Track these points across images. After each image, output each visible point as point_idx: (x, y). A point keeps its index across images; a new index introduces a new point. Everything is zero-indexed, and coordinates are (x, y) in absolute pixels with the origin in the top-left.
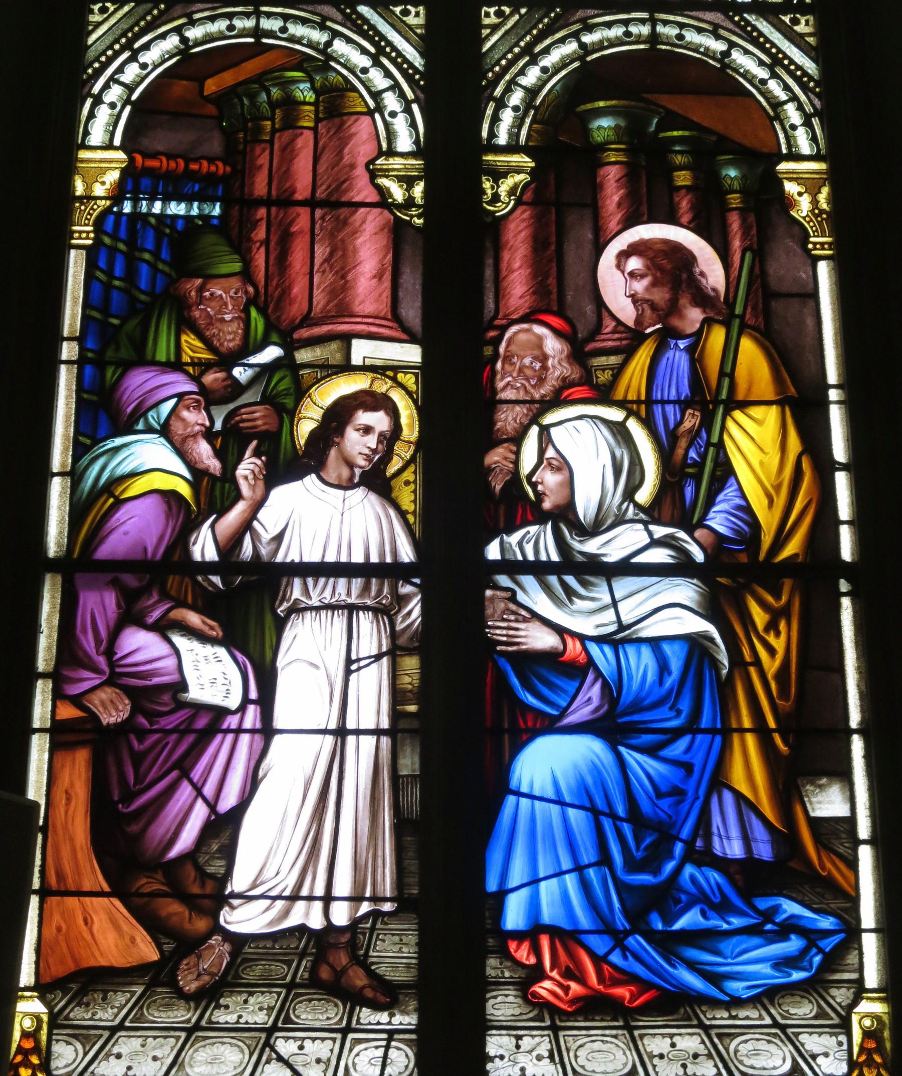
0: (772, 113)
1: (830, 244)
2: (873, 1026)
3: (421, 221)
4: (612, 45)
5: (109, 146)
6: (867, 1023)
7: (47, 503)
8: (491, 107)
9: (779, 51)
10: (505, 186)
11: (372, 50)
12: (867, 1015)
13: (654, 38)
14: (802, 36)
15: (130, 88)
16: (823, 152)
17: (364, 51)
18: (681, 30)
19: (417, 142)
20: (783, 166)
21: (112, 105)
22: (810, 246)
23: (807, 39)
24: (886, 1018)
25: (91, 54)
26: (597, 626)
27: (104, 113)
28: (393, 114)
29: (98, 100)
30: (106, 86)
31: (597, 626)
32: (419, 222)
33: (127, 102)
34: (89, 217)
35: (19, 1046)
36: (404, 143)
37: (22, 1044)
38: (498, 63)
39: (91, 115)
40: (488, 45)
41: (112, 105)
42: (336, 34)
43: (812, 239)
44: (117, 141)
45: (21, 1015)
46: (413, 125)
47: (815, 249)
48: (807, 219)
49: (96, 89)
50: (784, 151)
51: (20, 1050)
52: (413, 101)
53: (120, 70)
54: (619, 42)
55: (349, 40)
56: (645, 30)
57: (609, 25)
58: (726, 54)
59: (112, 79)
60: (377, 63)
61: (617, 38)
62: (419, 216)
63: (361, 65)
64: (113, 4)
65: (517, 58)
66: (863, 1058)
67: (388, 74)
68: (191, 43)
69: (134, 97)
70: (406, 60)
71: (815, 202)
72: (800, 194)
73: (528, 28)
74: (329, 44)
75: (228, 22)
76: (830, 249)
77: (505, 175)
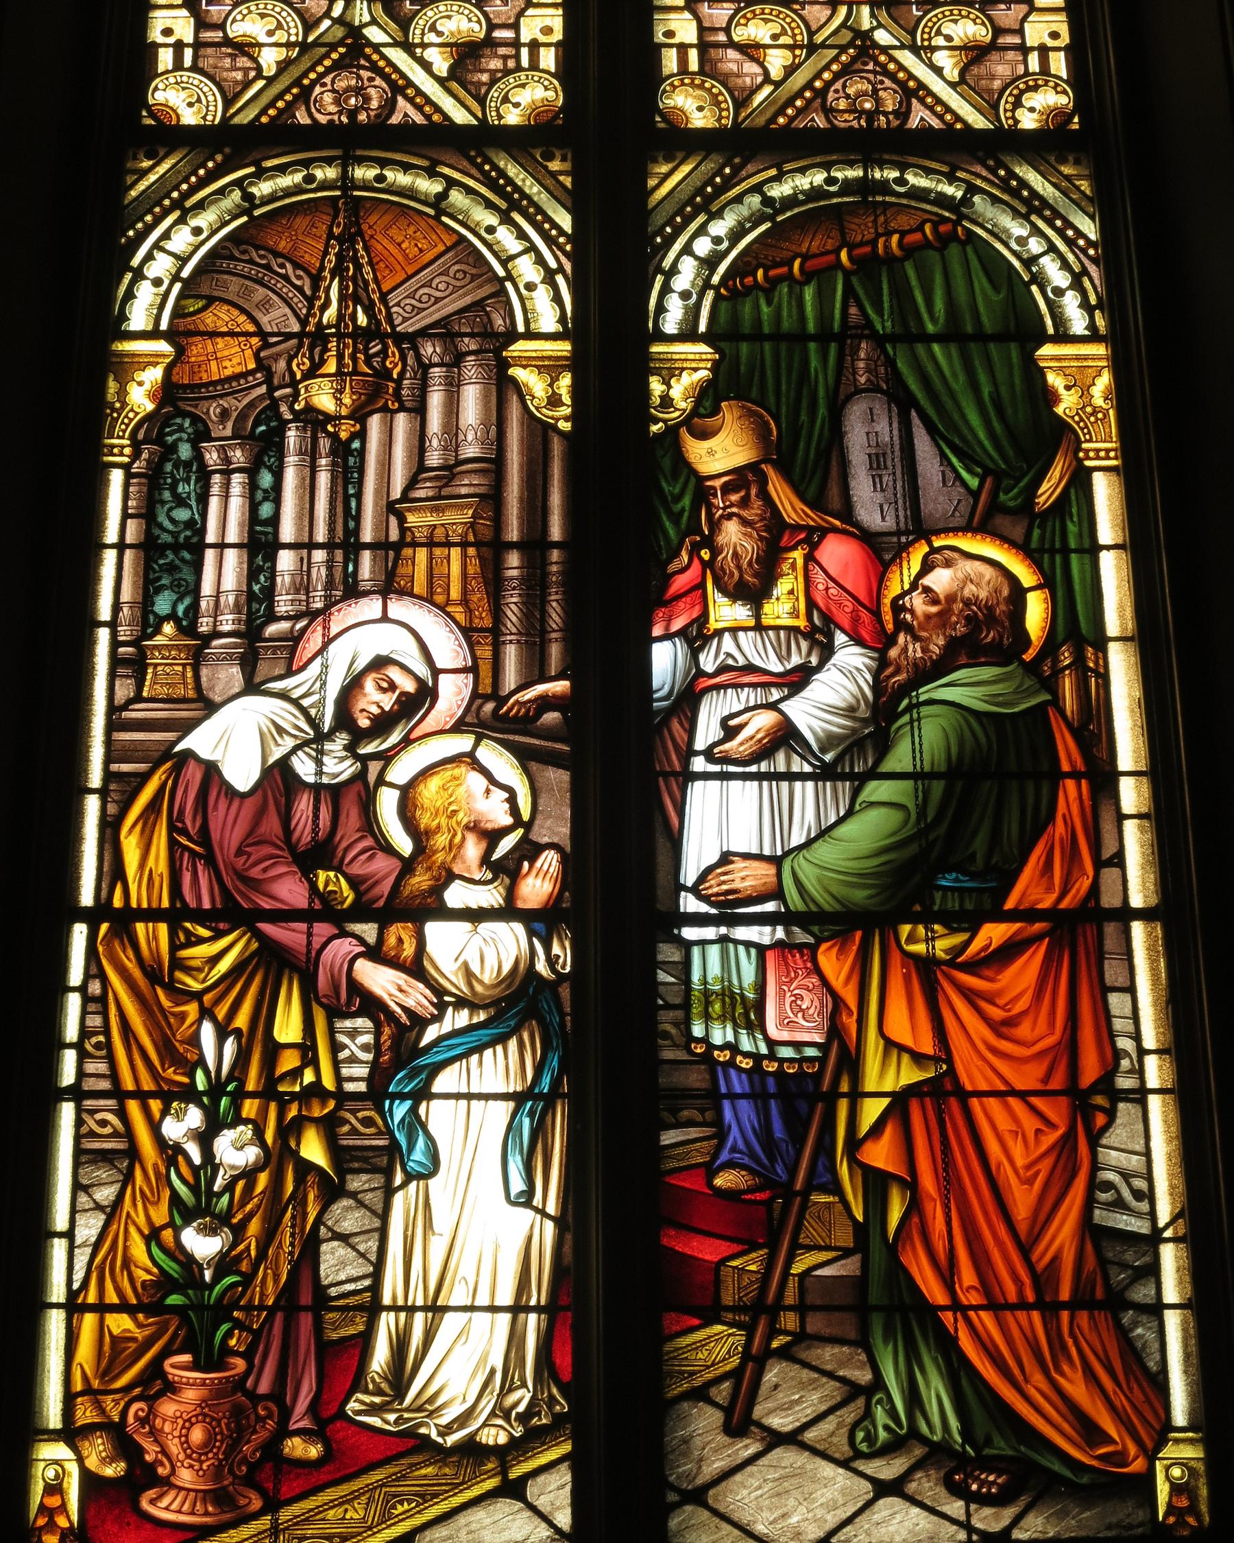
0: (501, 272)
1: (1115, 450)
2: (1182, 1478)
3: (569, 424)
6: (1176, 1472)
11: (503, 205)
12: (1178, 1462)
13: (346, 183)
14: (554, 175)
15: (183, 260)
17: (489, 205)
18: (829, 172)
19: (562, 320)
20: (1047, 350)
21: (157, 282)
22: (1081, 455)
23: (561, 178)
24: (1201, 1467)
26: (456, 959)
27: (146, 294)
28: (530, 287)
29: (139, 275)
30: (149, 257)
31: (456, 959)
32: (565, 426)
33: (176, 278)
35: (42, 1504)
36: (548, 321)
39: (130, 295)
41: (157, 282)
42: (451, 183)
43: (1085, 446)
45: (42, 1465)
46: (557, 299)
47: (1088, 458)
48: (1077, 418)
49: (135, 262)
50: (1051, 331)
51: (42, 1508)
52: (662, 272)
53: (166, 236)
54: (297, 190)
55: (469, 191)
56: (331, 173)
57: (282, 169)
58: (966, 201)
59: (157, 246)
60: (506, 220)
61: (296, 186)
62: (566, 419)
63: (487, 223)
65: (166, 212)
66: (1172, 1520)
67: (522, 235)
68: (257, 202)
74: (443, 196)
75: (378, 171)
76: (1116, 458)
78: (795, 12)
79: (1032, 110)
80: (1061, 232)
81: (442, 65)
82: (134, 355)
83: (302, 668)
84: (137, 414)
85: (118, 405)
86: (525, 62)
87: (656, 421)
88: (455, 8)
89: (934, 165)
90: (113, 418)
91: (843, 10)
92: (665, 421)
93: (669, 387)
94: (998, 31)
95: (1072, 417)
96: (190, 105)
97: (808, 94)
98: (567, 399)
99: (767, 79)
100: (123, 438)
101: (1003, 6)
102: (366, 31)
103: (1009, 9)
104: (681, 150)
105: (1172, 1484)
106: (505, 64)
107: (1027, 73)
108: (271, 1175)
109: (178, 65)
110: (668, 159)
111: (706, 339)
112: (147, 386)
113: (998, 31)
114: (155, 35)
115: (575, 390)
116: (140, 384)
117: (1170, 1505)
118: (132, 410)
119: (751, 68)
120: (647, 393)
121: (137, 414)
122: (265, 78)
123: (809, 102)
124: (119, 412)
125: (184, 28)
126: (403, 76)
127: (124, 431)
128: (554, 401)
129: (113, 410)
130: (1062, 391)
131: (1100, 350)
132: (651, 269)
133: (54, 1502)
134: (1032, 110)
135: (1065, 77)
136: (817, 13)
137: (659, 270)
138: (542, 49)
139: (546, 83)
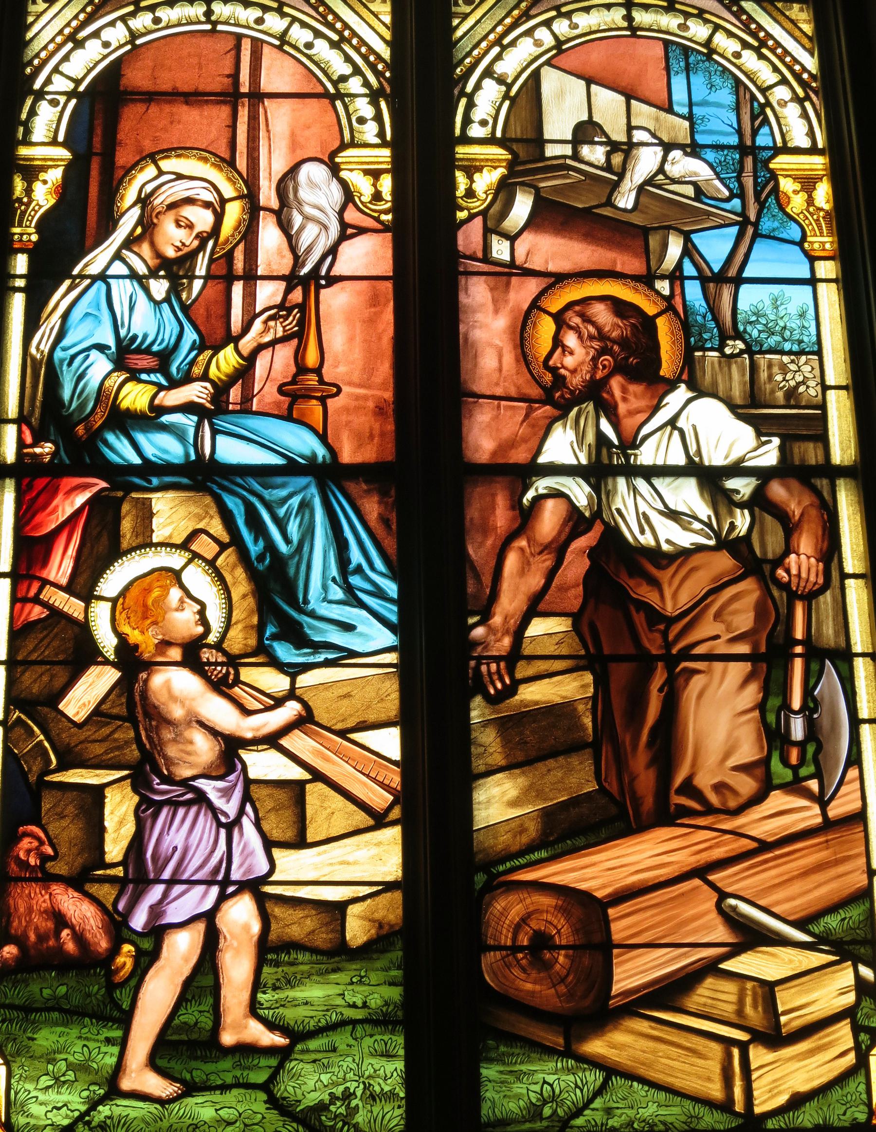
4: (190, 23)
5: (54, 142)
7: (846, 334)
8: (463, 102)
9: (346, 26)
16: (820, 145)
25: (30, 53)
34: (37, 208)
37: (108, 792)
38: (37, 55)
39: (33, 113)
40: (459, 33)
44: (61, 138)
59: (56, 70)
69: (81, 88)
70: (371, 50)
71: (810, 201)
72: (796, 192)
73: (508, 9)
77: (480, 169)
80: (781, 59)
83: (494, 595)
84: (41, 207)
85: (25, 200)
87: (462, 209)
92: (468, 209)
93: (472, 181)
95: (798, 215)
98: (389, 198)
100: (30, 227)
108: (397, 512)
110: (384, 520)
111: (64, 145)
112: (50, 185)
115: (395, 192)
116: (45, 182)
118: (38, 204)
120: (452, 185)
121: (41, 207)
124: (28, 205)
127: (31, 222)
128: (377, 196)
129: (22, 203)
132: (456, 92)
137: (462, 93)
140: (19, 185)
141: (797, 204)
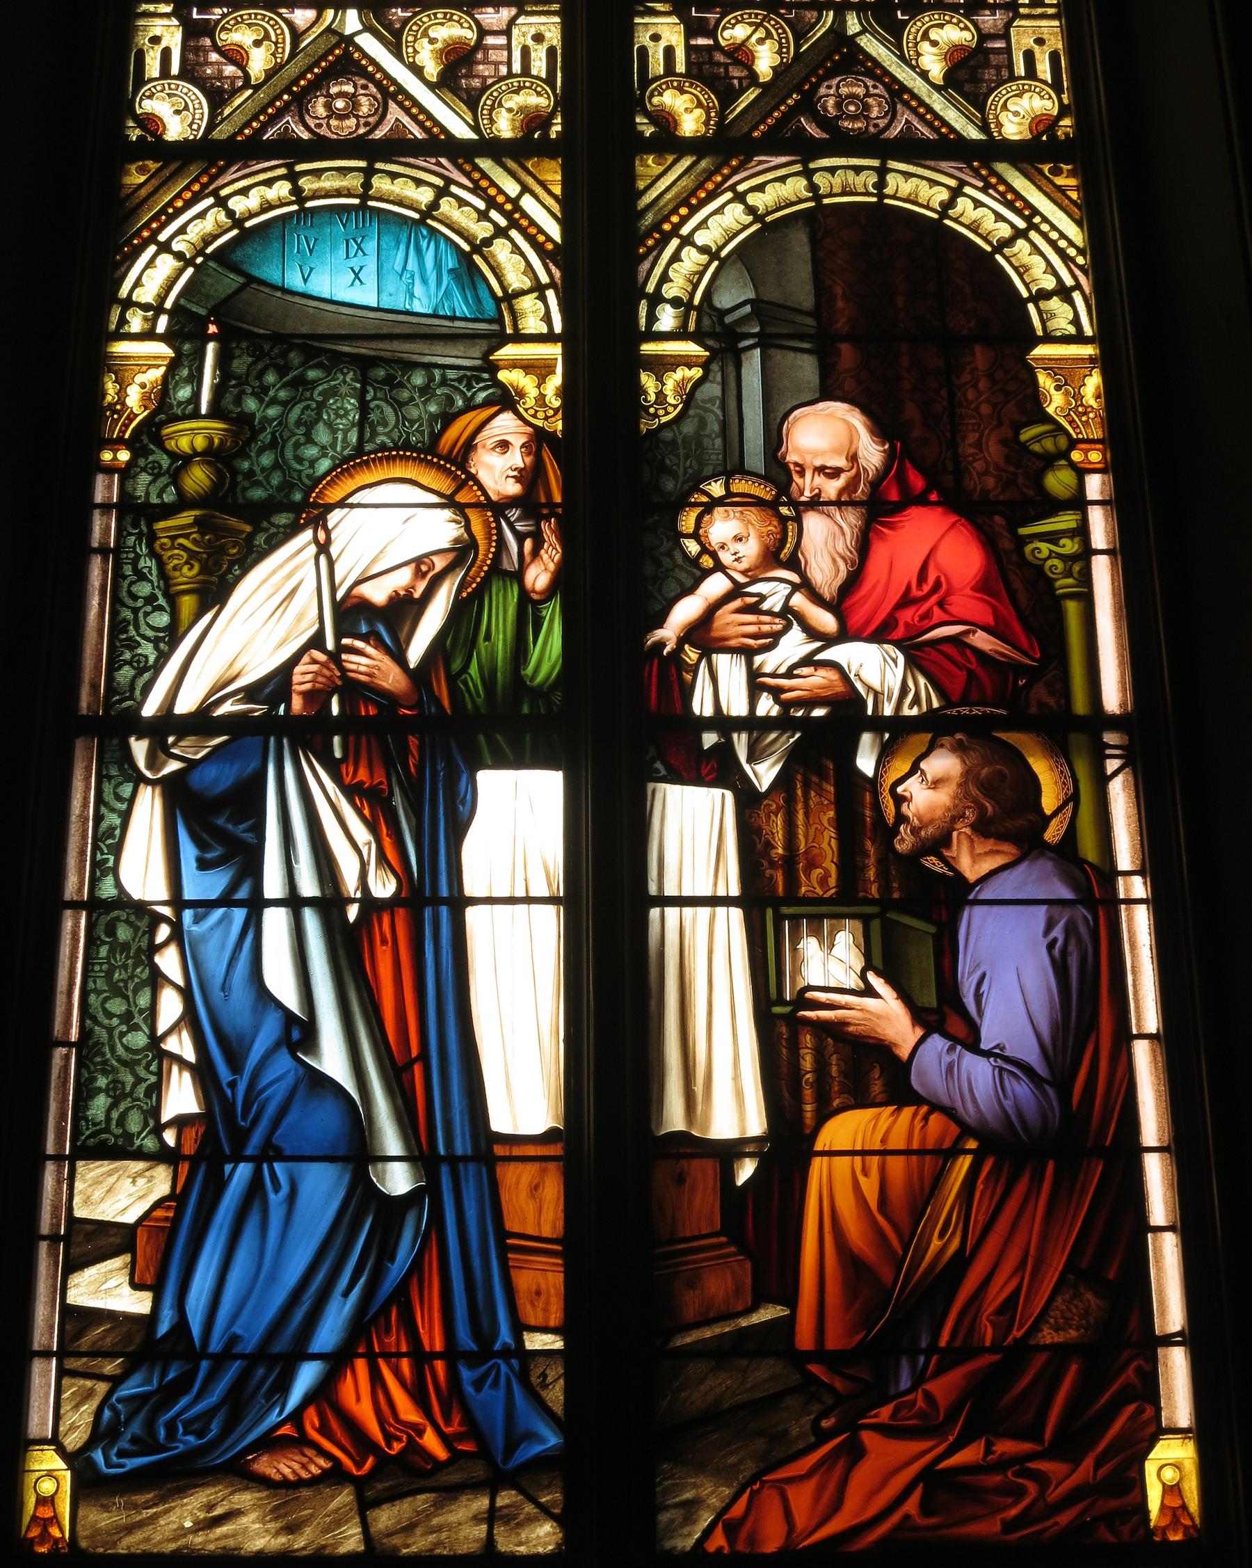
10: (672, 380)
14: (1060, 189)
64: (156, 161)
78: (280, 15)
79: (1016, 114)
81: (432, 70)
82: (128, 358)
86: (1020, 69)
88: (947, 18)
89: (920, 171)
90: (113, 419)
91: (330, 13)
94: (483, 32)
96: (177, 112)
97: (286, 97)
99: (247, 83)
101: (490, 10)
102: (358, 39)
103: (498, 12)
104: (672, 153)
105: (1164, 1484)
106: (497, 70)
107: (510, 75)
109: (165, 73)
111: (165, 338)
113: (483, 32)
114: (143, 40)
117: (1163, 1507)
119: (230, 70)
120: (640, 390)
122: (758, 85)
123: (287, 104)
125: (172, 37)
126: (394, 82)
130: (1053, 391)
131: (1088, 350)
133: (46, 1513)
134: (1016, 114)
135: (1050, 82)
136: (302, 17)
138: (490, 52)
139: (539, 89)
140: (111, 388)
141: (1055, 403)
